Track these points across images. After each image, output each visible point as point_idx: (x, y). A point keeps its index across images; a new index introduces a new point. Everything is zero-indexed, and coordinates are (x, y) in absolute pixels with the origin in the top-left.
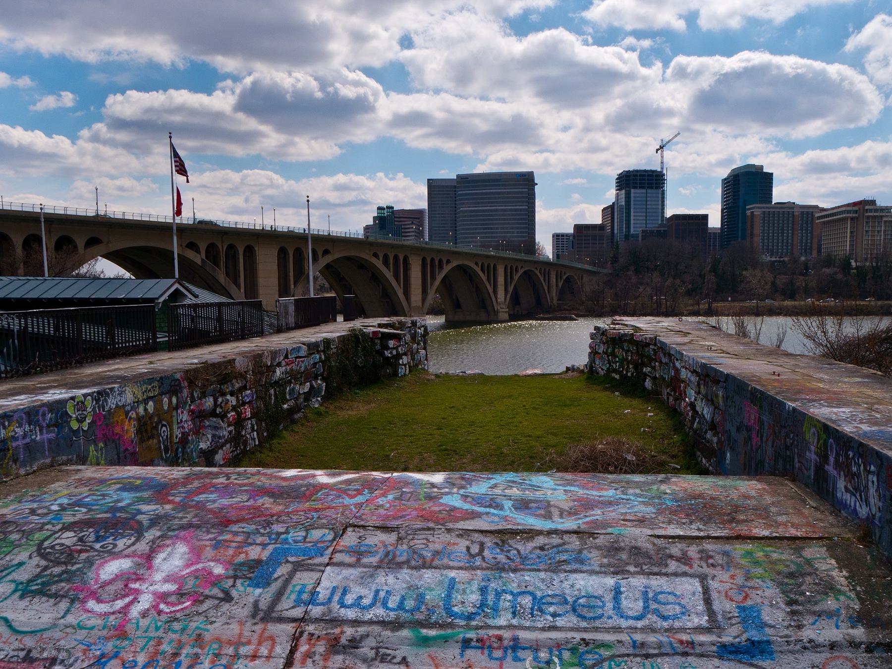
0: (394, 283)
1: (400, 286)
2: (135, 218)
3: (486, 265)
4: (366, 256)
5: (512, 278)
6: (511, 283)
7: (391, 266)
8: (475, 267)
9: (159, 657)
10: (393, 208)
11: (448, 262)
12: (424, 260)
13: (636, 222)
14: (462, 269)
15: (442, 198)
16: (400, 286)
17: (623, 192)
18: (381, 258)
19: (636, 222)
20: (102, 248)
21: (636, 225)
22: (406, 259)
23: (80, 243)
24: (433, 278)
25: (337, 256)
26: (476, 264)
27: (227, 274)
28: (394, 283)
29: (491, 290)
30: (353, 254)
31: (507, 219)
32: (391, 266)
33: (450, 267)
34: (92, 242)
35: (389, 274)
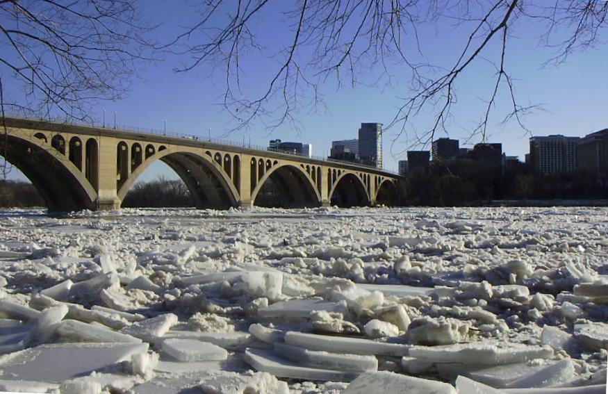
5: (261, 174)
6: (334, 182)
8: (301, 169)
11: (275, 163)
26: (302, 165)
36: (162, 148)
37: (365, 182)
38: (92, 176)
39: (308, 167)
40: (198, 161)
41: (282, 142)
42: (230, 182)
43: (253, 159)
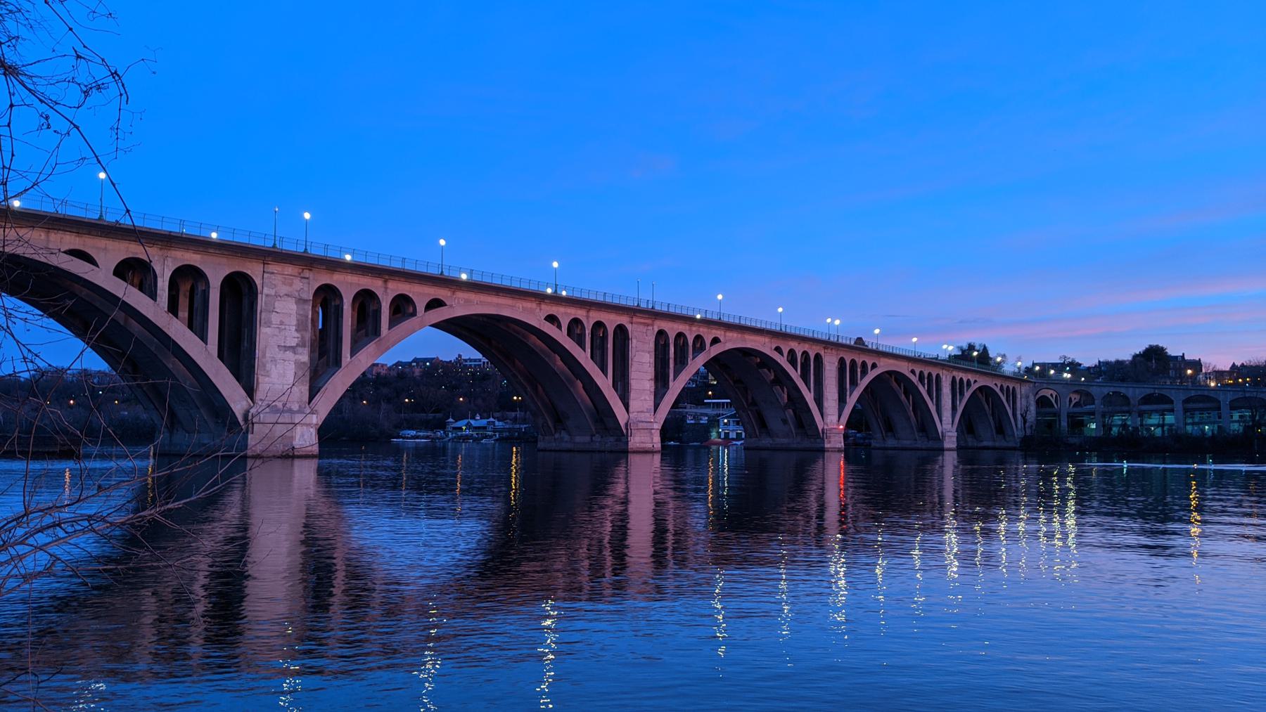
1: (810, 391)
5: (962, 394)
11: (874, 366)
28: (986, 406)
42: (809, 397)
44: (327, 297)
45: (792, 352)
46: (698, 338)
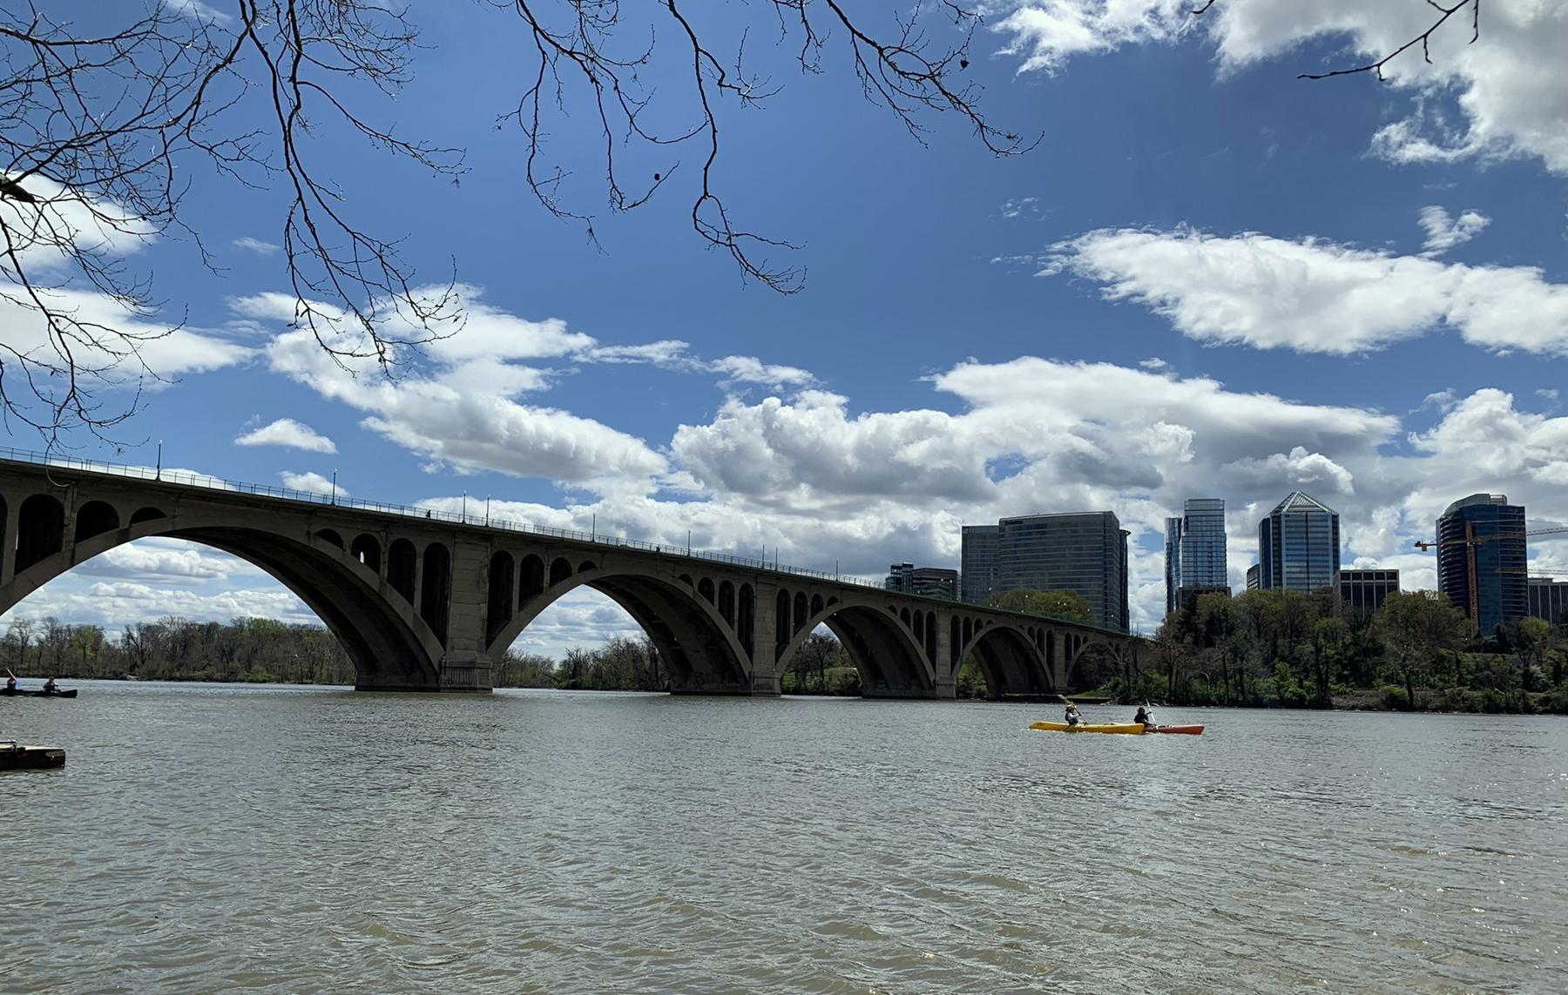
0: (722, 623)
1: (922, 645)
2: (676, 553)
3: (962, 620)
4: (881, 608)
7: (912, 623)
8: (890, 614)
9: (1288, 695)
10: (911, 566)
12: (1068, 638)
13: (1326, 558)
14: (1003, 633)
15: (1045, 544)
16: (922, 645)
17: (1434, 220)
18: (899, 614)
19: (1326, 558)
20: (590, 574)
21: (1288, 524)
22: (931, 617)
23: (124, 512)
24: (967, 637)
25: (846, 605)
27: (721, 610)
28: (722, 623)
29: (1044, 661)
30: (640, 573)
31: (1084, 567)
32: (912, 623)
33: (990, 627)
34: (586, 566)
35: (909, 632)
36: (832, 601)
37: (918, 635)
38: (435, 613)
39: (905, 612)
40: (647, 583)
41: (915, 568)
42: (922, 652)
43: (784, 593)
44: (499, 567)
45: (905, 612)
46: (817, 598)
